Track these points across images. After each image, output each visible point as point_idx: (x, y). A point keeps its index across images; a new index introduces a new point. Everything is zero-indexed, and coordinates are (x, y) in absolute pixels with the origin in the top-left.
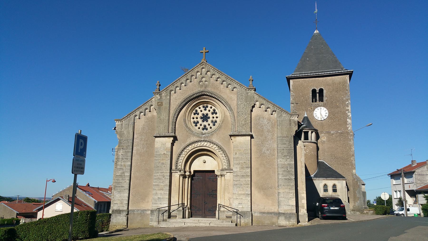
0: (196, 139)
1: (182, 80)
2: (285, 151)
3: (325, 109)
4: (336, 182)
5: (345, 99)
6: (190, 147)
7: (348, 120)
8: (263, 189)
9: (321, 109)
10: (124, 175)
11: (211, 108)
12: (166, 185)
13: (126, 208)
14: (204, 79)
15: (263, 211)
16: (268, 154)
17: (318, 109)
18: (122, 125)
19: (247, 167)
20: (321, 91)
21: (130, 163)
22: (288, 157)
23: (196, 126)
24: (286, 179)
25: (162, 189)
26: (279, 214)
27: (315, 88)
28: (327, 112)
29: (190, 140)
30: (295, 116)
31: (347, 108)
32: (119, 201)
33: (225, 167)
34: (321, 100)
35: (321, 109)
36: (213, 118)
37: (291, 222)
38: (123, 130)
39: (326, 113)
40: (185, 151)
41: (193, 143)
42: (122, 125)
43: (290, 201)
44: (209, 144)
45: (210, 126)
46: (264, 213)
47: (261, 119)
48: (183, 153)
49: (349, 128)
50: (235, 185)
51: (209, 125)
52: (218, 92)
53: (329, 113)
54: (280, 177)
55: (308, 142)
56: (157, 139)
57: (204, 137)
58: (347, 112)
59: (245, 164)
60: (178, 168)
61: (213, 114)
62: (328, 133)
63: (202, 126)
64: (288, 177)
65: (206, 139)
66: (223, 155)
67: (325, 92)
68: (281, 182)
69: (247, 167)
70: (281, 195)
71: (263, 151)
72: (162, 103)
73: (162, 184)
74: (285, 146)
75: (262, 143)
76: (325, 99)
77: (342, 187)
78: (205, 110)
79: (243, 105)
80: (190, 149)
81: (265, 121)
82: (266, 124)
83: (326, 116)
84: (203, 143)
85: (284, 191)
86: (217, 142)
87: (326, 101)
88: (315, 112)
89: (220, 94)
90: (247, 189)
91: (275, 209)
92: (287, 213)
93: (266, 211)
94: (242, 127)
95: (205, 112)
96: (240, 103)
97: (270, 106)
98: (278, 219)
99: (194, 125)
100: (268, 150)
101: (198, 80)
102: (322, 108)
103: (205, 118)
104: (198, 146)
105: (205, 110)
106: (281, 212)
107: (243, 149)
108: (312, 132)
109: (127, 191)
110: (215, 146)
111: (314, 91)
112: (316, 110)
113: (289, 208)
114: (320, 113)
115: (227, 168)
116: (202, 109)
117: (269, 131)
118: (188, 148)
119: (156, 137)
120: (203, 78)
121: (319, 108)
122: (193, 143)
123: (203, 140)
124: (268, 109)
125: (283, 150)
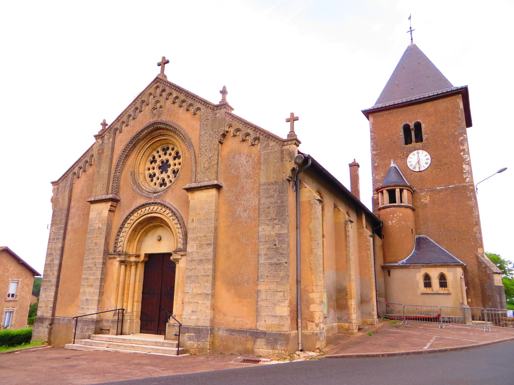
0: (143, 201)
1: (130, 111)
2: (271, 210)
3: (425, 153)
4: (445, 271)
5: (457, 133)
6: (136, 214)
7: (464, 166)
8: (235, 284)
9: (418, 153)
10: (53, 264)
11: (173, 149)
12: (97, 279)
13: (49, 315)
14: (158, 105)
15: (232, 326)
16: (246, 218)
17: (414, 155)
18: (58, 188)
19: (208, 244)
20: (418, 126)
21: (60, 245)
22: (275, 221)
23: (152, 181)
24: (271, 264)
25: (92, 286)
26: (256, 334)
27: (407, 123)
28: (429, 157)
29: (136, 203)
30: (289, 143)
31: (461, 147)
32: (44, 304)
33: (180, 246)
34: (419, 138)
35: (418, 153)
36: (175, 165)
37: (276, 351)
38: (58, 196)
39: (427, 159)
40: (129, 221)
41: (138, 208)
42: (58, 188)
43: (277, 308)
44: (160, 208)
45: (170, 179)
46: (234, 331)
47: (237, 156)
48: (126, 226)
49: (467, 179)
50: (189, 277)
51: (169, 177)
52: (175, 121)
53: (432, 158)
54: (262, 260)
55: (394, 206)
56: (94, 207)
57: (155, 197)
58: (462, 153)
59: (205, 238)
60: (118, 250)
61: (175, 159)
62: (433, 191)
63: (160, 181)
64: (275, 261)
65: (158, 201)
66: (179, 226)
67: (423, 126)
68: (264, 271)
69: (208, 244)
70: (263, 296)
71: (238, 213)
72: (103, 149)
73: (92, 277)
74: (272, 200)
75: (236, 199)
76: (424, 137)
77: (455, 277)
78: (165, 154)
79: (207, 135)
80: (135, 218)
81: (243, 158)
82: (245, 163)
83: (427, 163)
84: (152, 207)
85: (267, 288)
86: (172, 203)
87: (427, 139)
88: (409, 160)
89: (177, 123)
90: (206, 284)
91: (248, 324)
92: (270, 334)
93: (237, 328)
94: (204, 173)
95: (164, 158)
96: (203, 132)
97: (249, 131)
98: (255, 342)
99: (149, 179)
100: (245, 211)
101: (150, 107)
102: (421, 151)
103: (164, 166)
104: (146, 212)
105: (165, 154)
106: (260, 329)
107: (204, 212)
108: (401, 191)
109: (54, 288)
110: (168, 211)
111: (407, 129)
112: (411, 155)
113: (276, 321)
114: (419, 160)
115: (182, 247)
116: (161, 153)
117: (248, 177)
118: (132, 218)
119: (92, 202)
120: (157, 102)
121: (415, 152)
122: (138, 208)
123: (152, 201)
124: (247, 138)
125: (269, 208)
